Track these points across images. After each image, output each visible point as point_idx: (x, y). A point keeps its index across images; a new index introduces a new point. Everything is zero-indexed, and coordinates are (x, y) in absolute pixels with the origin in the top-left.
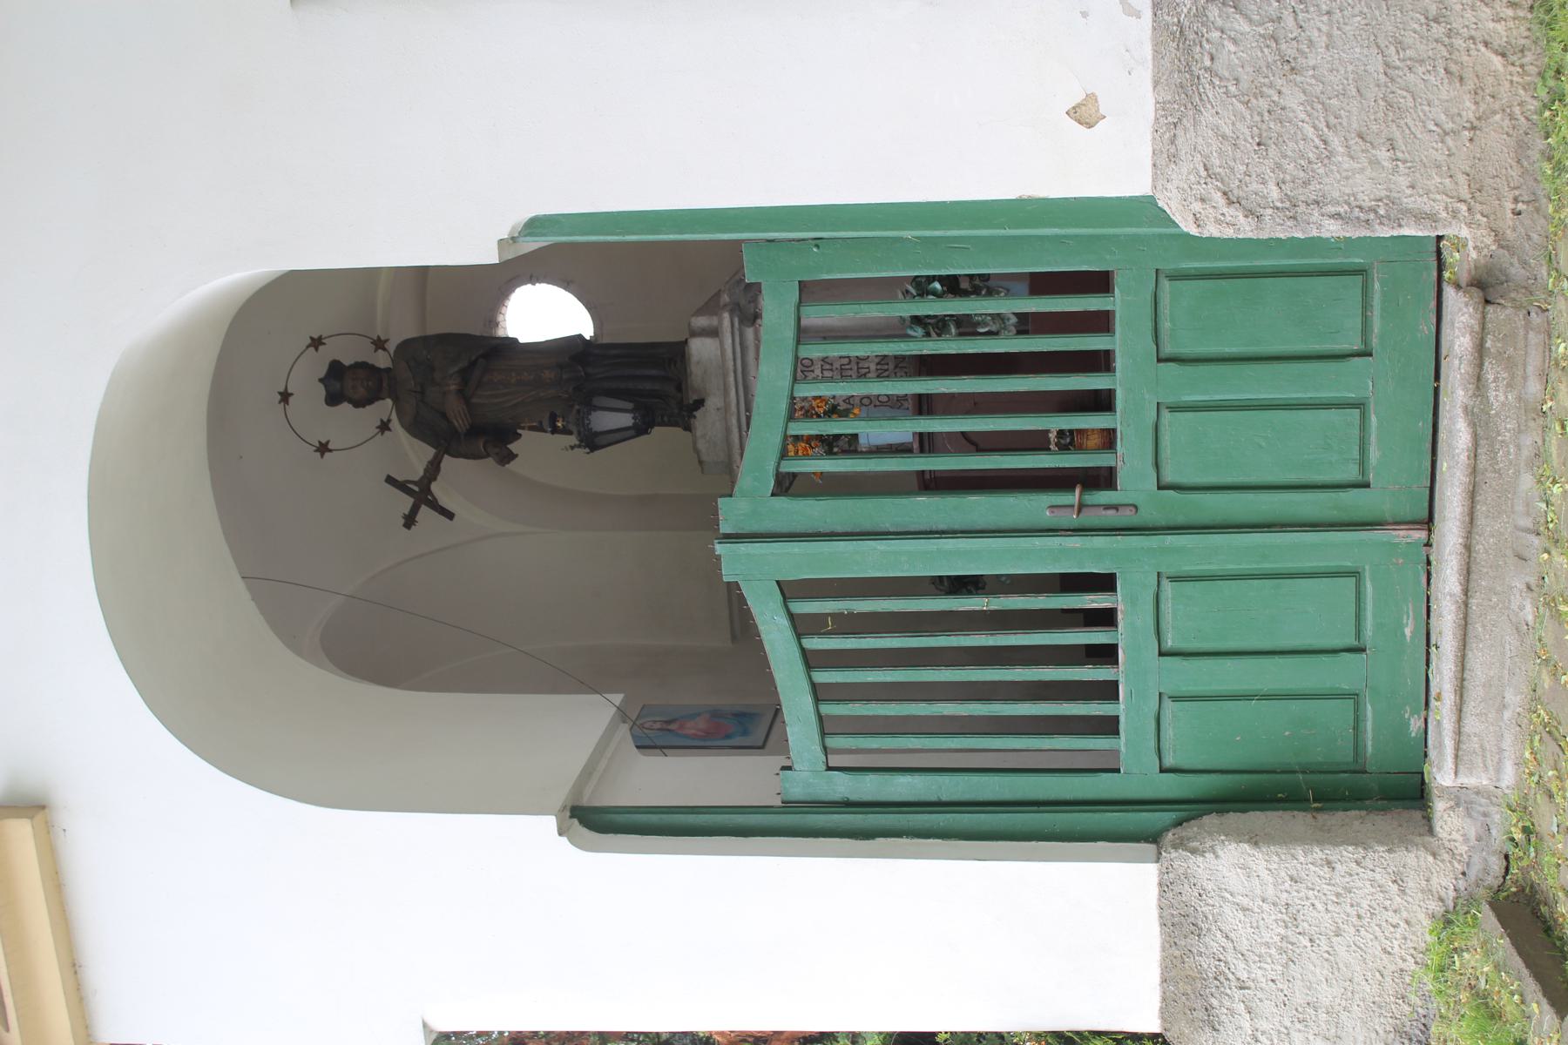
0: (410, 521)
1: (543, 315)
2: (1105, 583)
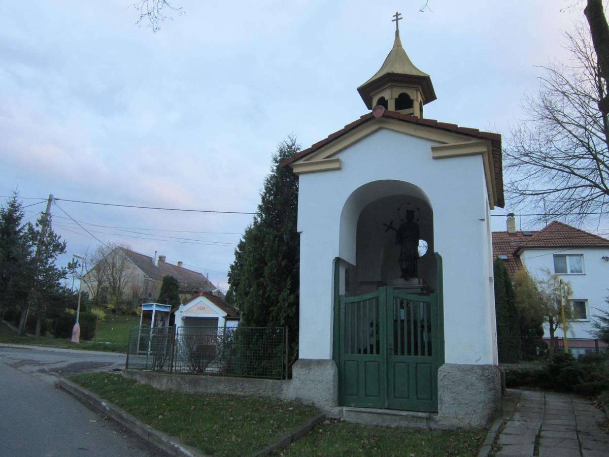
0: (385, 224)
1: (422, 248)
2: (378, 352)
